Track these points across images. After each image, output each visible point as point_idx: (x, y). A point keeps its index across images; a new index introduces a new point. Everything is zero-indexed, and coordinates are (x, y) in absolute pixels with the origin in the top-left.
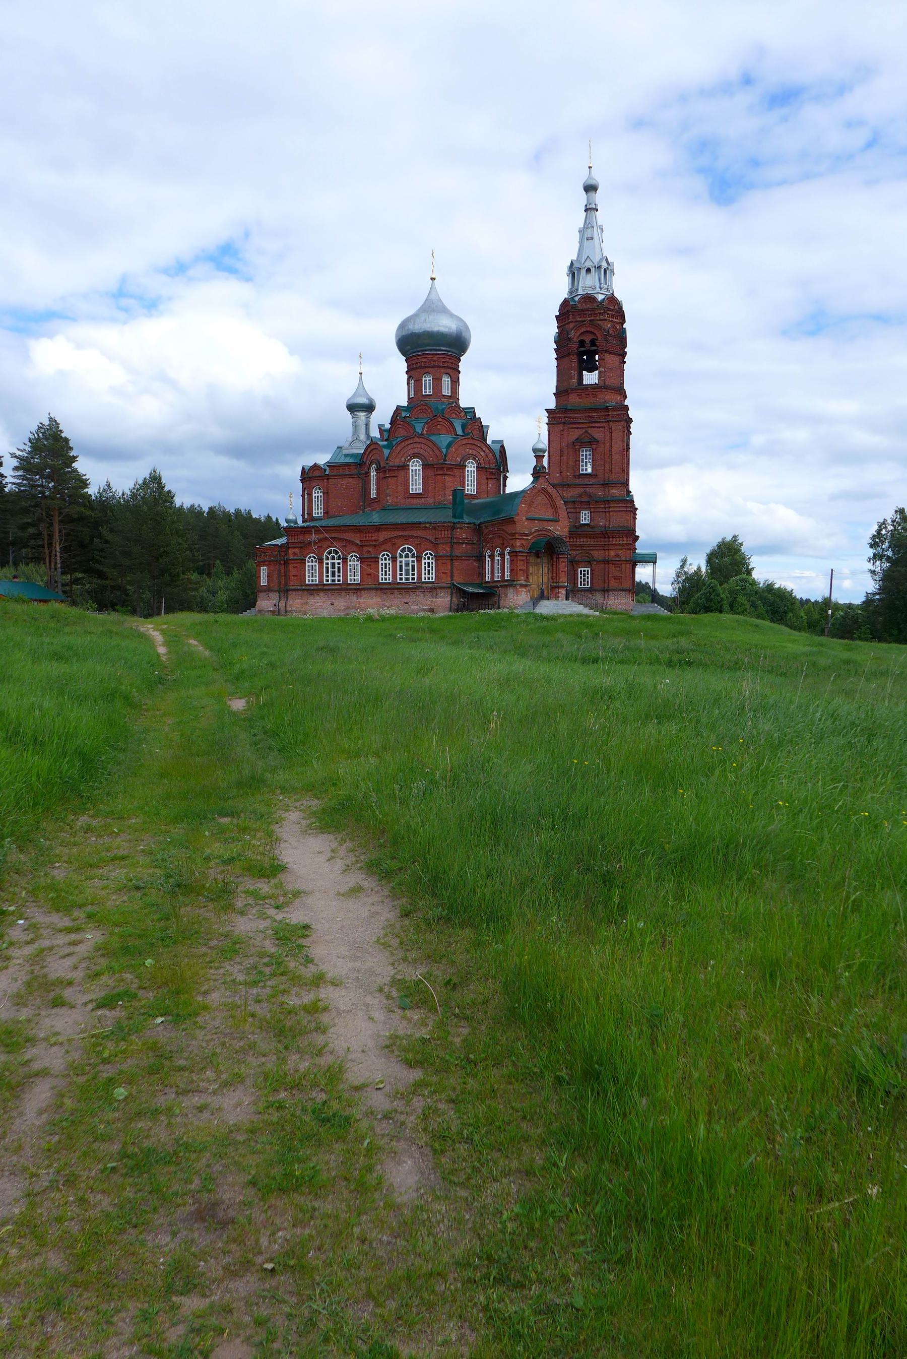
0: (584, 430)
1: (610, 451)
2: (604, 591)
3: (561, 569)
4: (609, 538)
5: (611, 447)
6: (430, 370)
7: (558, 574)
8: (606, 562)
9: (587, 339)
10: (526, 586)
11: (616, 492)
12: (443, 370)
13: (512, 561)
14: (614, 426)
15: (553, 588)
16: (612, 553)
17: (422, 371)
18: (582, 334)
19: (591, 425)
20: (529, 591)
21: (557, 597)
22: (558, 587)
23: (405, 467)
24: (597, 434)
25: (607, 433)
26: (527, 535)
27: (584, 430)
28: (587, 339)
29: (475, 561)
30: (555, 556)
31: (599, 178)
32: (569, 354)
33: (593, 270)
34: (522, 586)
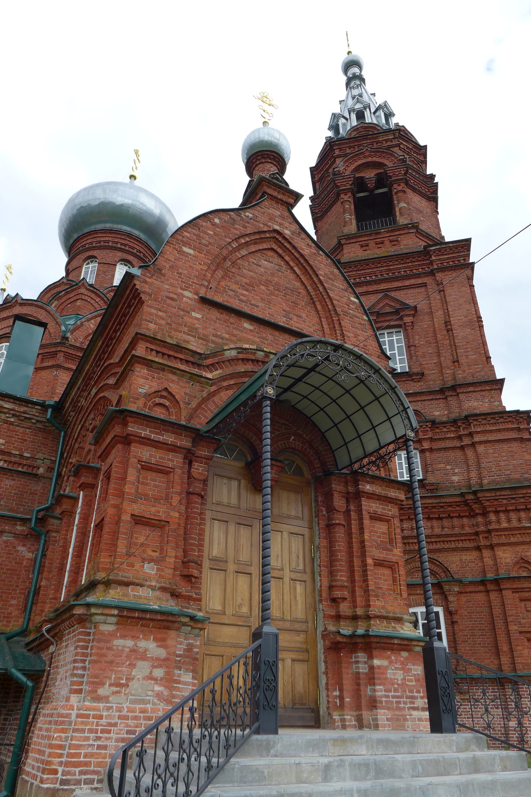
0: (380, 296)
1: (447, 323)
2: (501, 682)
3: (374, 553)
4: (485, 514)
5: (447, 314)
6: (95, 253)
7: (358, 577)
8: (492, 583)
9: (370, 175)
10: (160, 623)
11: (475, 404)
12: (119, 254)
14: (445, 278)
15: (341, 648)
16: (506, 556)
18: (358, 169)
19: (396, 284)
20: (192, 660)
21: (363, 708)
22: (369, 644)
24: (409, 298)
25: (436, 297)
26: (196, 359)
27: (380, 296)
28: (370, 175)
29: (23, 538)
30: (337, 487)
31: (358, 53)
32: (338, 195)
34: (134, 618)
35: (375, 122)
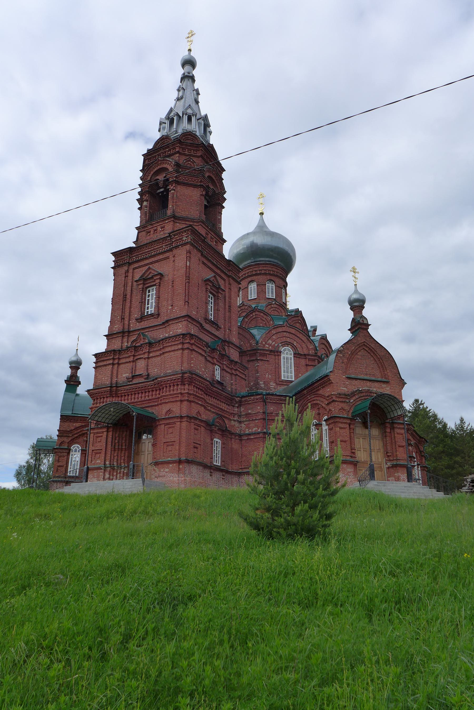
12: (265, 277)
13: (330, 429)
23: (277, 353)
24: (158, 268)
33: (193, 119)
35: (198, 134)
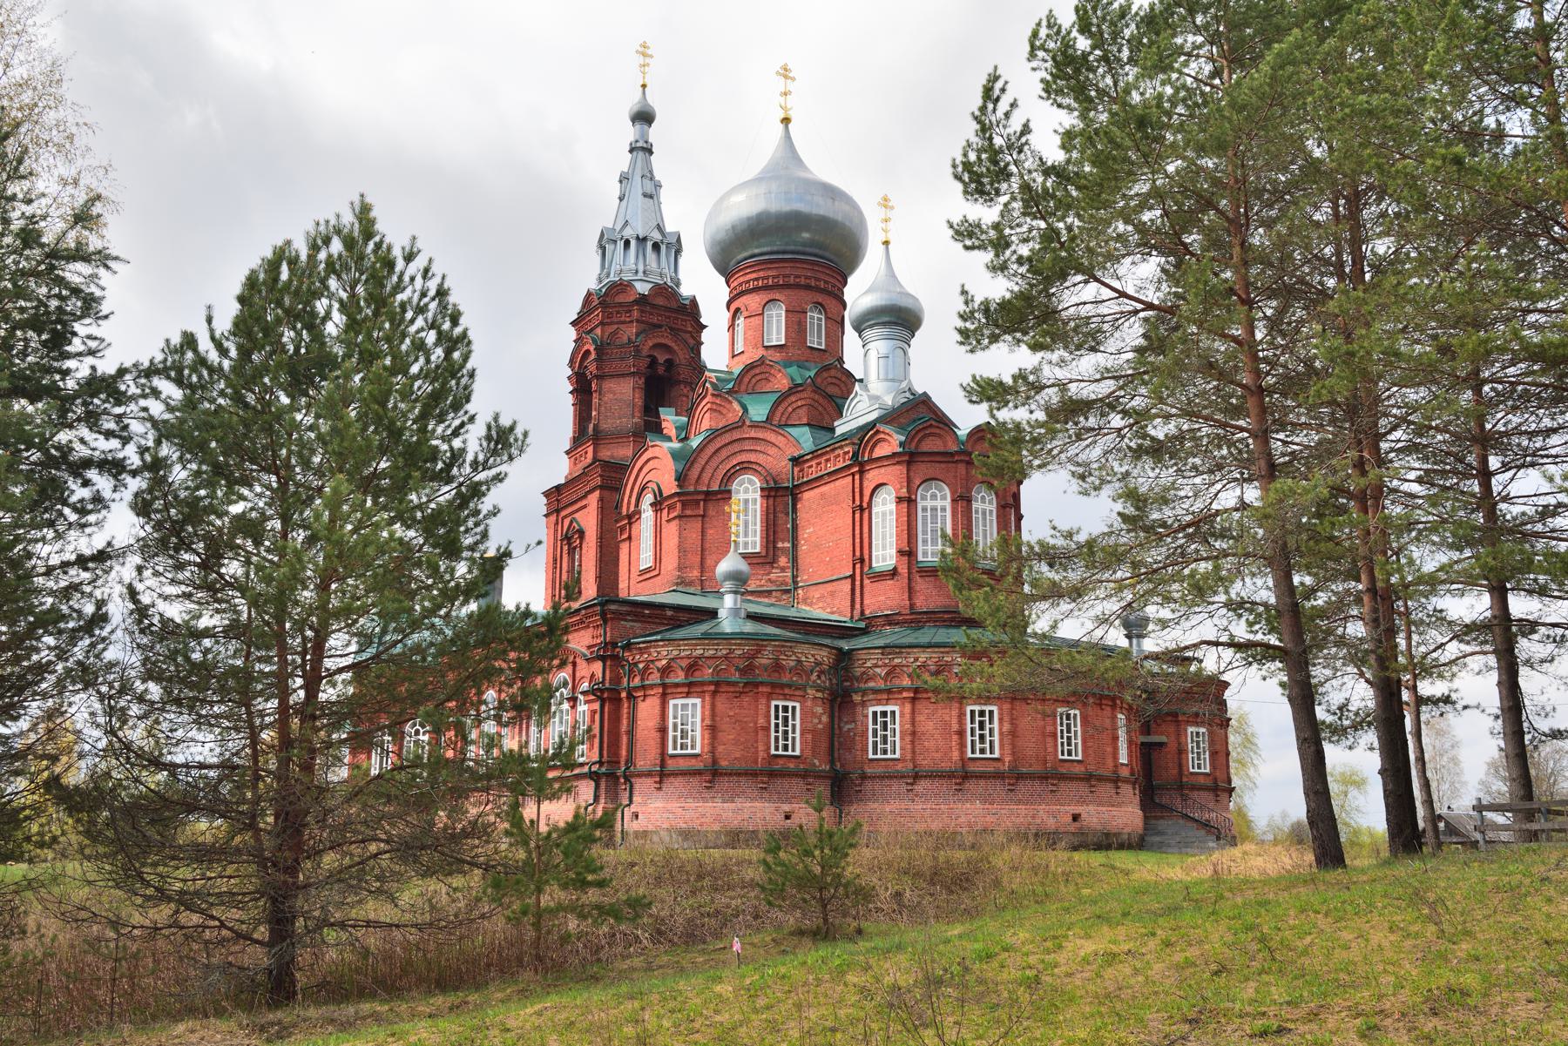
17: (765, 296)
23: (725, 495)
31: (655, 102)
